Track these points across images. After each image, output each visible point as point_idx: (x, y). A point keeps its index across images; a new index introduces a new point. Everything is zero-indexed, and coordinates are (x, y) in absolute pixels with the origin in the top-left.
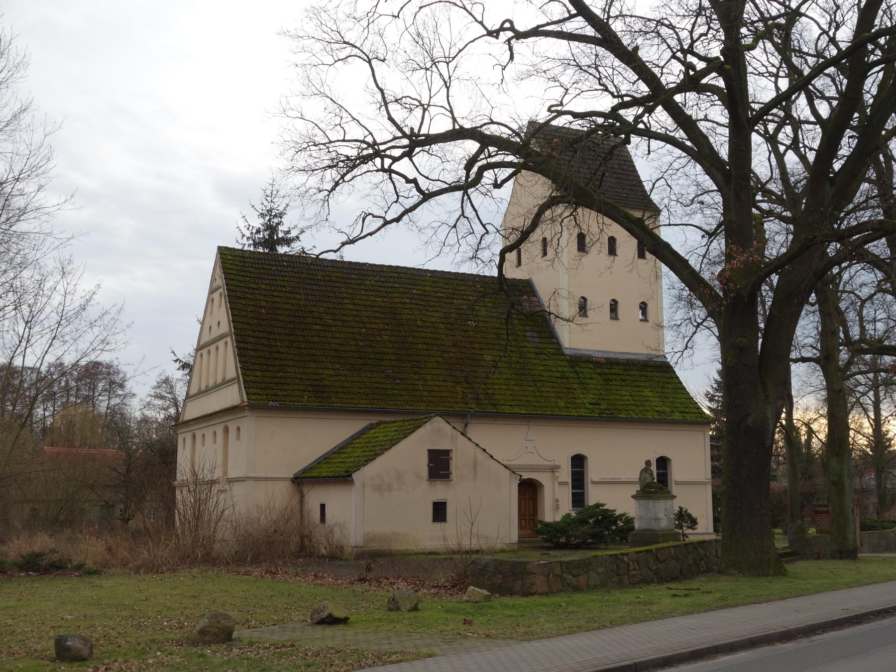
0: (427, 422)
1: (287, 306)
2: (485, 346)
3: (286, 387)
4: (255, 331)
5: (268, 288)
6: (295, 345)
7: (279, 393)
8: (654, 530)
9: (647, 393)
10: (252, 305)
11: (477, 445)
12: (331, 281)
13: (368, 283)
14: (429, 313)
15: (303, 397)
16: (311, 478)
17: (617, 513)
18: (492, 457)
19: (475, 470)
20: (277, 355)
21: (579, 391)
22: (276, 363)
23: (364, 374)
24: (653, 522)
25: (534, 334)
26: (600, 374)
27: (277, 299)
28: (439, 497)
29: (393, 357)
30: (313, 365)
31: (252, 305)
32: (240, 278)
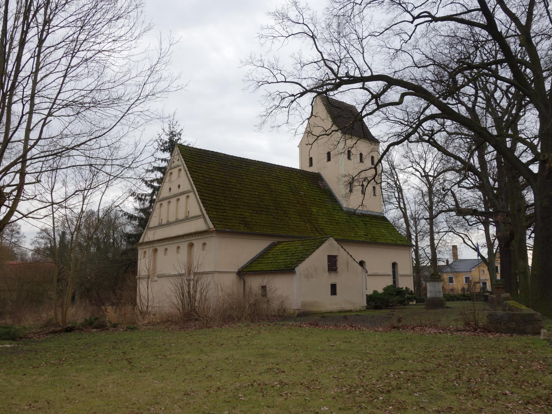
0: (326, 240)
1: (218, 178)
2: (311, 205)
3: (230, 221)
4: (206, 190)
5: (206, 167)
6: (227, 199)
7: (228, 224)
8: (439, 298)
9: (383, 230)
10: (201, 176)
11: (348, 253)
12: (235, 167)
13: (251, 169)
14: (283, 186)
15: (240, 227)
16: (255, 271)
17: (380, 291)
18: (354, 260)
19: (348, 267)
20: (220, 204)
21: (357, 229)
22: (221, 208)
23: (263, 216)
24: (438, 294)
25: (329, 200)
26: (361, 221)
27: (212, 174)
28: (333, 281)
29: (274, 208)
30: (239, 210)
31: (201, 176)
32: (191, 161)
